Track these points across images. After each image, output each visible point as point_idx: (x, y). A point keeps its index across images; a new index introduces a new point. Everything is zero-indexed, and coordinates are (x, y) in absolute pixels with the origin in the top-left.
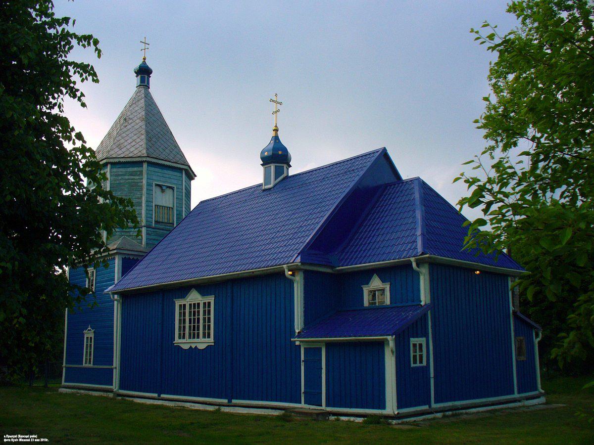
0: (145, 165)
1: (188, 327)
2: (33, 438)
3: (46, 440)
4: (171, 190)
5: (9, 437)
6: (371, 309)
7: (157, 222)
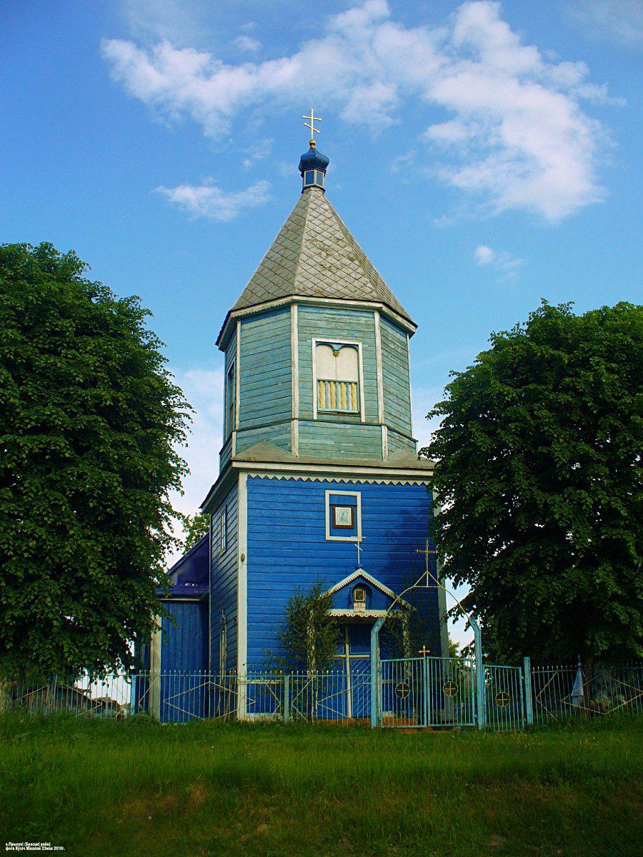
0: (295, 309)
1: (380, 688)
2: (46, 846)
3: (62, 848)
4: (351, 351)
5: (12, 845)
6: (232, 334)
7: (319, 413)
